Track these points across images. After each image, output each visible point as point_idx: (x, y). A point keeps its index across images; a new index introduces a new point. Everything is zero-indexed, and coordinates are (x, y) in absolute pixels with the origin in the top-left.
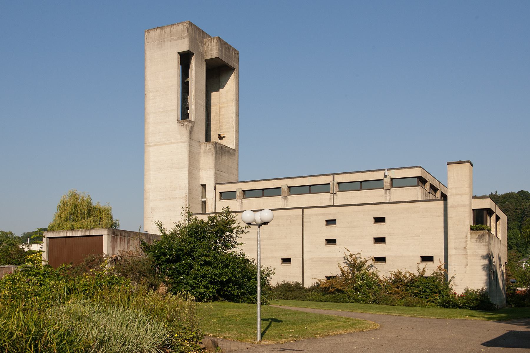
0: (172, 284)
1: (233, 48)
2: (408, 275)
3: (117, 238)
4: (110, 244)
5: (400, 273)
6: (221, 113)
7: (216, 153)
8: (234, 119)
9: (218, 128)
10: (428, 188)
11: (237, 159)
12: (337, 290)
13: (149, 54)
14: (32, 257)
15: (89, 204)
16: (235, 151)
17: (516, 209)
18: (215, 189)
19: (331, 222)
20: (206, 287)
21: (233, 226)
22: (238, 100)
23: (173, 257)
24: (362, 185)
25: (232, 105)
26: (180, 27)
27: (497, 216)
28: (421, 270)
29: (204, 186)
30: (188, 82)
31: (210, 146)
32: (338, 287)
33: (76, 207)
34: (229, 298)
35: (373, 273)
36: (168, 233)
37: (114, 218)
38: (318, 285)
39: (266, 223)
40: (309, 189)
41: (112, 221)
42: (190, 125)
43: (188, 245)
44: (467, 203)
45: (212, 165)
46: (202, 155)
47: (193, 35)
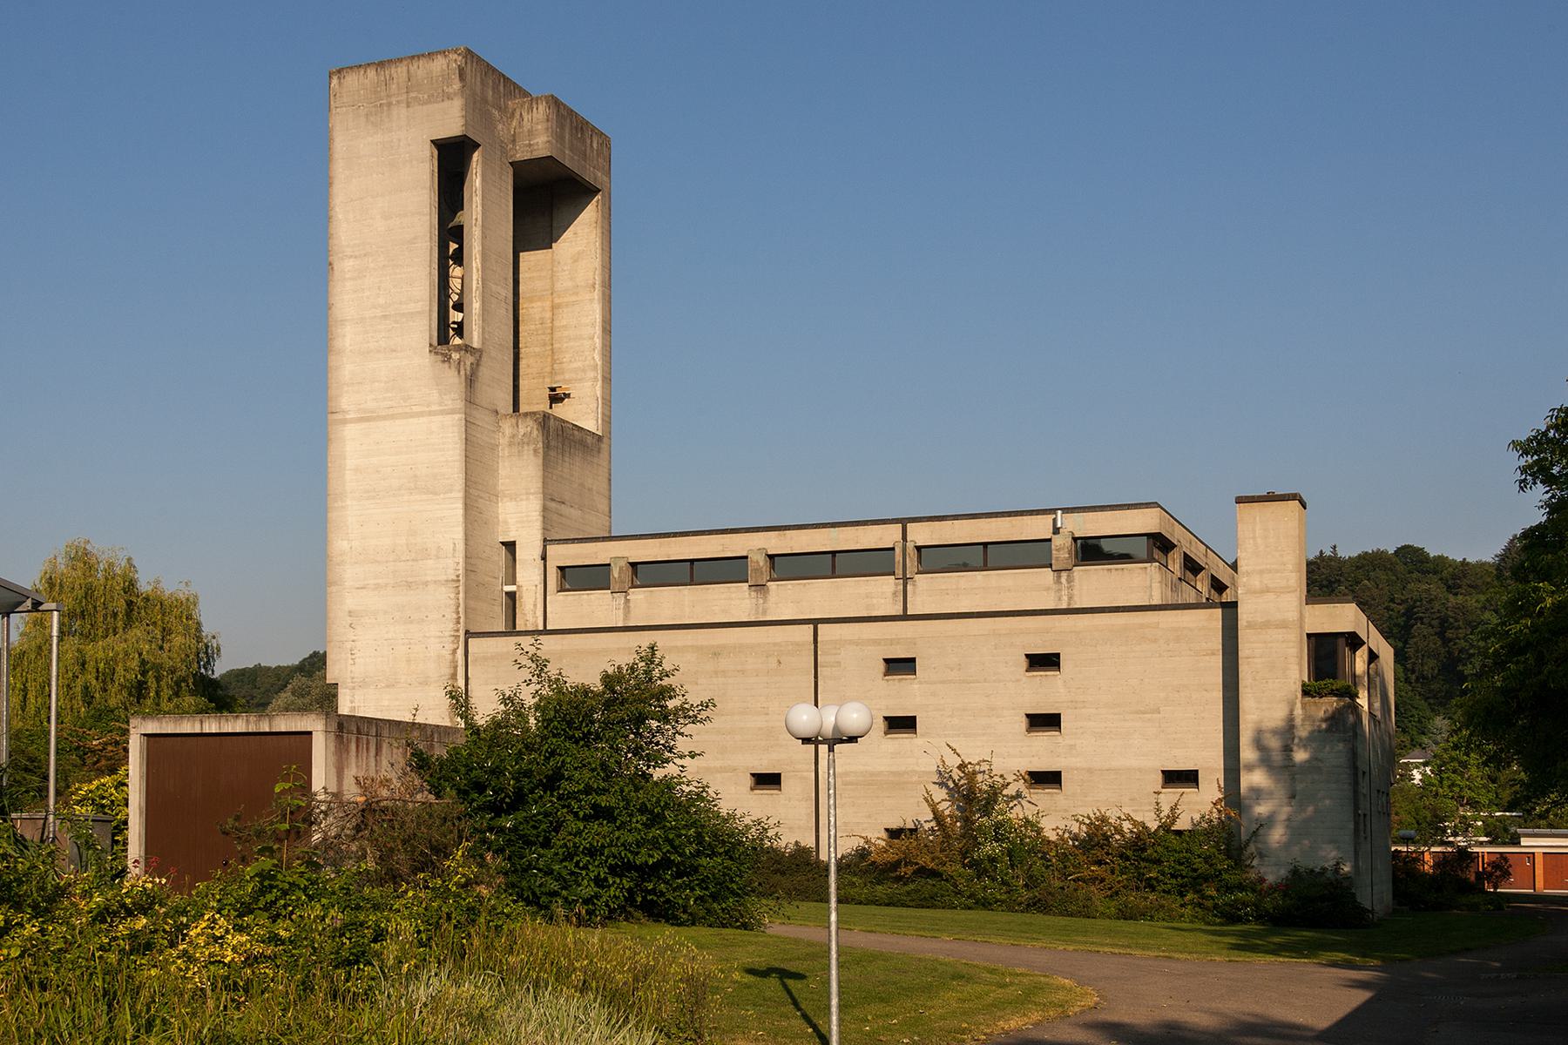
0: (506, 874)
1: (594, 129)
2: (1126, 826)
3: (349, 741)
4: (332, 759)
5: (1104, 820)
6: (556, 323)
7: (547, 446)
8: (598, 342)
9: (548, 369)
10: (1177, 566)
11: (605, 464)
12: (923, 872)
13: (341, 143)
14: (92, 787)
15: (130, 586)
16: (600, 438)
17: (1392, 600)
18: (544, 558)
19: (900, 666)
20: (600, 882)
21: (671, 704)
22: (608, 285)
23: (507, 796)
24: (987, 556)
25: (591, 300)
26: (439, 64)
27: (1370, 651)
28: (1166, 811)
29: (510, 546)
30: (460, 228)
31: (528, 427)
32: (925, 860)
33: (89, 592)
34: (660, 912)
35: (1028, 821)
36: (481, 721)
37: (207, 630)
38: (862, 854)
39: (852, 739)
40: (832, 564)
41: (199, 639)
42: (469, 360)
43: (547, 759)
44: (1292, 615)
45: (536, 485)
46: (503, 451)
47: (478, 90)
